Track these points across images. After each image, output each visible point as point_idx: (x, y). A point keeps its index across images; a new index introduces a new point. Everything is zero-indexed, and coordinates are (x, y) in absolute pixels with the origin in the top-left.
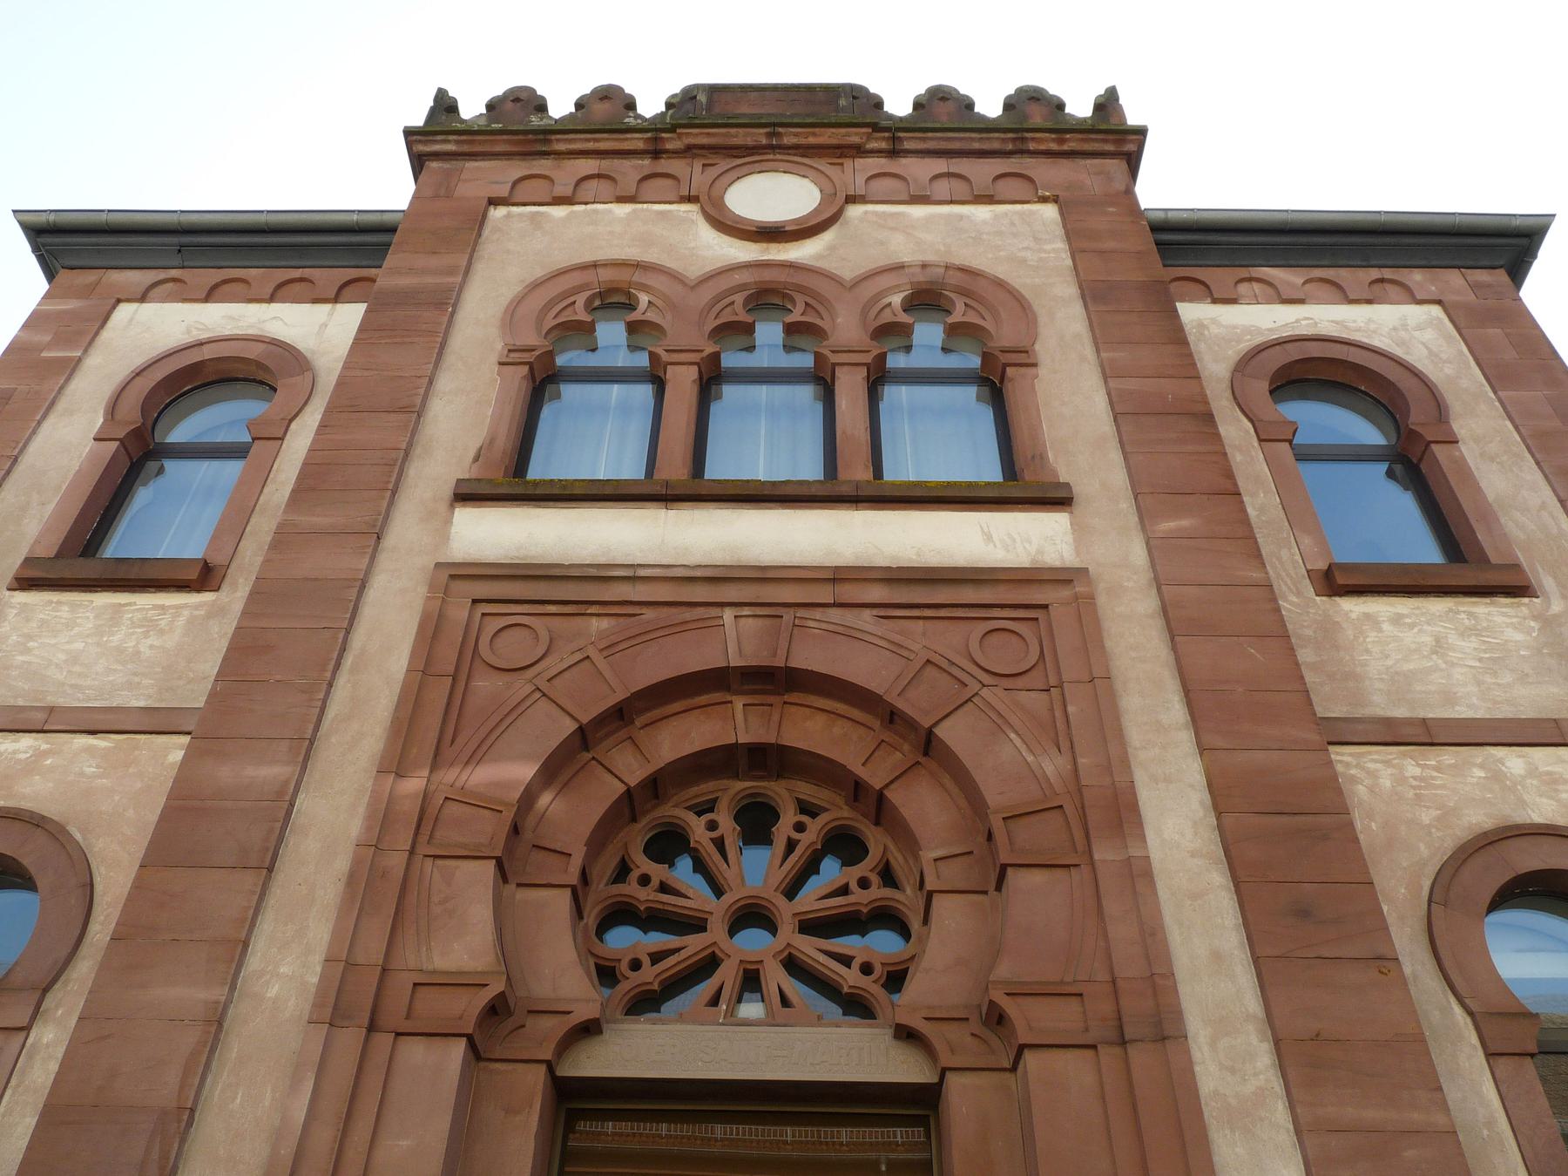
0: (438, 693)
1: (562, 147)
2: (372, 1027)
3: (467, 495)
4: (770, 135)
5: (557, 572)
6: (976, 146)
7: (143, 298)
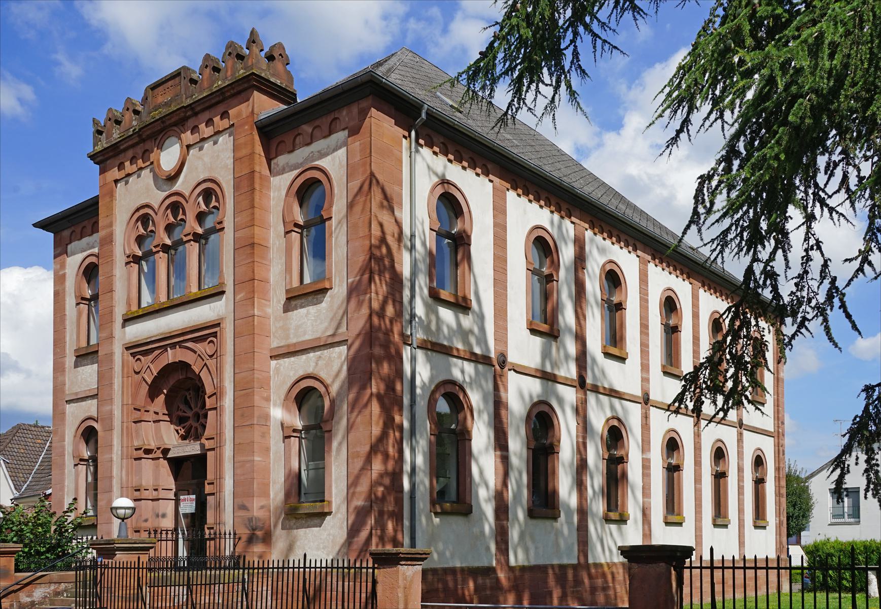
1: (122, 147)
4: (163, 122)
5: (139, 343)
6: (213, 101)
7: (71, 242)
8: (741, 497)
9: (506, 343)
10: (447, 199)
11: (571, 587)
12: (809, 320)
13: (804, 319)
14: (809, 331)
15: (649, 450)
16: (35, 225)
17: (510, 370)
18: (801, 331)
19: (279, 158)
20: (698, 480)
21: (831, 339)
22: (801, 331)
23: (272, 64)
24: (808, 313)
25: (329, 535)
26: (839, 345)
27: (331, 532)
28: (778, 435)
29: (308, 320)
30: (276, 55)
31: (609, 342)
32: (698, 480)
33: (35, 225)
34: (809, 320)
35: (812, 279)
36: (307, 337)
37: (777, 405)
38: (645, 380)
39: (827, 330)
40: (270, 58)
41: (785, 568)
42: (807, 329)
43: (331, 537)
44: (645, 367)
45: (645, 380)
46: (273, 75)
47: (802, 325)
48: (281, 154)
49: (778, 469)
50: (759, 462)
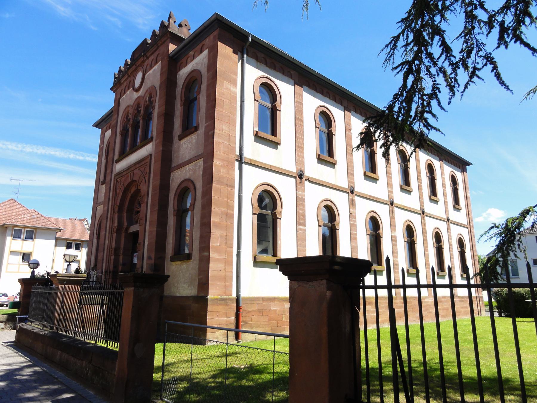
0: (114, 192)
1: (122, 82)
2: (111, 233)
3: (118, 161)
7: (106, 132)
8: (452, 260)
9: (303, 163)
10: (264, 85)
11: (67, 334)
12: (478, 69)
13: (475, 69)
14: (481, 78)
15: (395, 230)
16: (472, 164)
17: (306, 180)
18: (472, 80)
19: (181, 71)
20: (426, 249)
21: (502, 83)
22: (472, 80)
23: (180, 28)
24: (478, 63)
25: (190, 274)
26: (511, 88)
27: (191, 272)
28: (469, 227)
29: (187, 150)
30: (183, 25)
31: (368, 169)
32: (426, 249)
33: (472, 164)
34: (478, 69)
35: (479, 33)
36: (186, 160)
37: (468, 211)
38: (390, 192)
39: (498, 76)
40: (180, 25)
41: (427, 286)
42: (478, 77)
43: (191, 275)
44: (390, 185)
45: (390, 192)
46: (181, 33)
47: (473, 74)
48: (181, 70)
49: (474, 259)
50: (461, 243)
